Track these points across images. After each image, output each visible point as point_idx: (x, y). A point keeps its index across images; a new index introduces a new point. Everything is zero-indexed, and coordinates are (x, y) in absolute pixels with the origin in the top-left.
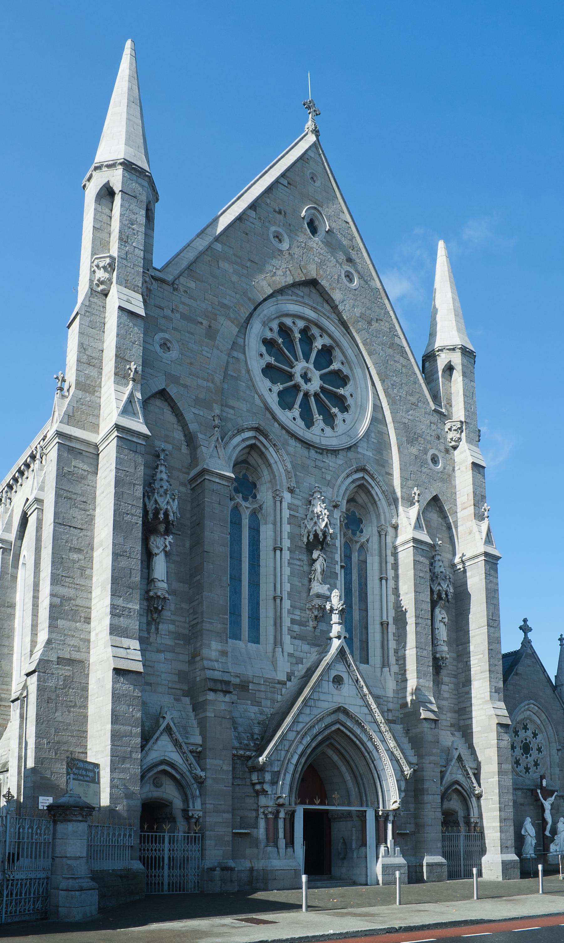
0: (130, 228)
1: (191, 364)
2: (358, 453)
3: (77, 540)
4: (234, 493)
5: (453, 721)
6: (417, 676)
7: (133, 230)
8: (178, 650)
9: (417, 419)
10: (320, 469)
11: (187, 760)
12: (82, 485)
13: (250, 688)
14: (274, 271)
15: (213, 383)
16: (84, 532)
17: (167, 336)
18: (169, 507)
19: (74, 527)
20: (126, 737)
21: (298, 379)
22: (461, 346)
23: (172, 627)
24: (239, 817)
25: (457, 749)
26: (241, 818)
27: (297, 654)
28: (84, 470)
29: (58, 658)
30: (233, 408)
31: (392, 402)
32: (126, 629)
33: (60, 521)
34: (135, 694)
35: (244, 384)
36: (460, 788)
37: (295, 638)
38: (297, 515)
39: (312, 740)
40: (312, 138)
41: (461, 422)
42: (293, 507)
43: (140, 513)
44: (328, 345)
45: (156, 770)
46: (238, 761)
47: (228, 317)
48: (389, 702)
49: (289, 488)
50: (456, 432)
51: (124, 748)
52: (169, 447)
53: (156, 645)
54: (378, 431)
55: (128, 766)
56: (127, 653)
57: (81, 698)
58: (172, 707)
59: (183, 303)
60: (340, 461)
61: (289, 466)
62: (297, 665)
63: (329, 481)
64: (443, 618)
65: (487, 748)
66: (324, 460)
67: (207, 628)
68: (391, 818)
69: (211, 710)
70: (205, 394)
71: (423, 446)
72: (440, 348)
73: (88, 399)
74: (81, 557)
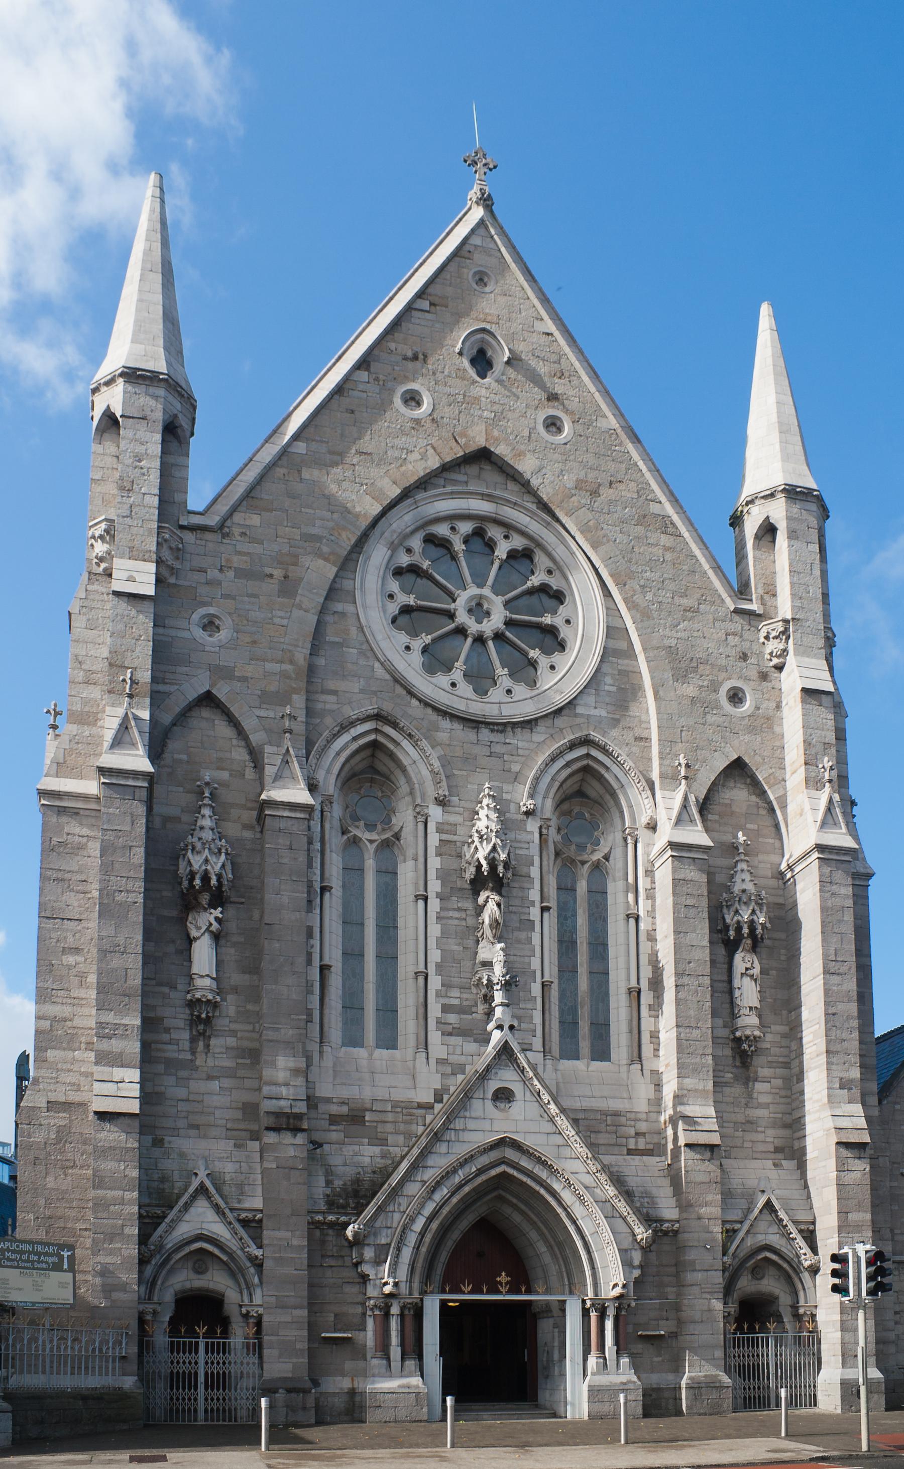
0: (135, 467)
1: (254, 642)
2: (576, 715)
3: (74, 936)
4: (349, 821)
5: (779, 1143)
6: (678, 1073)
7: (142, 468)
8: (241, 1073)
9: (695, 634)
10: (500, 756)
11: (236, 1234)
12: (79, 858)
13: (367, 1118)
14: (404, 456)
15: (291, 662)
16: (84, 924)
17: (212, 610)
18: (209, 867)
19: (69, 919)
20: (115, 1205)
21: (463, 617)
22: (783, 487)
23: (231, 1041)
24: (333, 1315)
25: (763, 1191)
26: (336, 1316)
27: (453, 1059)
28: (83, 836)
29: (48, 1102)
30: (335, 693)
31: (643, 615)
32: (121, 1054)
33: (48, 914)
34: (129, 1145)
35: (355, 651)
36: (774, 1257)
37: (450, 1034)
38: (455, 838)
39: (453, 1194)
40: (478, 213)
41: (786, 621)
42: (446, 827)
43: (140, 887)
44: (520, 549)
45: (187, 1250)
46: (330, 1232)
47: (320, 555)
48: (640, 1120)
49: (436, 798)
50: (778, 640)
51: (111, 1221)
52: (225, 775)
53: (205, 1069)
54: (619, 671)
55: (118, 1245)
56: (118, 1089)
57: (82, 1155)
58: (227, 1158)
59: (239, 553)
60: (538, 737)
61: (437, 764)
62: (453, 1077)
63: (517, 773)
64: (747, 969)
65: (826, 1186)
66: (507, 741)
67: (270, 1038)
68: (611, 1312)
69: (271, 1158)
70: (277, 683)
71: (710, 677)
72: (749, 499)
73: (87, 733)
74: (80, 959)
